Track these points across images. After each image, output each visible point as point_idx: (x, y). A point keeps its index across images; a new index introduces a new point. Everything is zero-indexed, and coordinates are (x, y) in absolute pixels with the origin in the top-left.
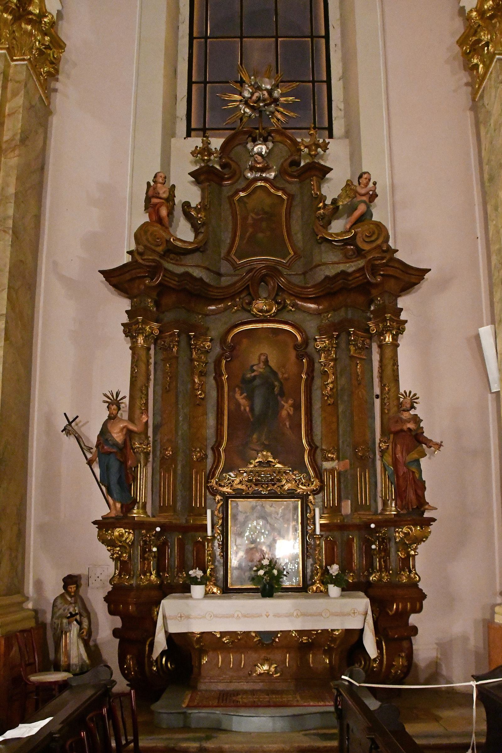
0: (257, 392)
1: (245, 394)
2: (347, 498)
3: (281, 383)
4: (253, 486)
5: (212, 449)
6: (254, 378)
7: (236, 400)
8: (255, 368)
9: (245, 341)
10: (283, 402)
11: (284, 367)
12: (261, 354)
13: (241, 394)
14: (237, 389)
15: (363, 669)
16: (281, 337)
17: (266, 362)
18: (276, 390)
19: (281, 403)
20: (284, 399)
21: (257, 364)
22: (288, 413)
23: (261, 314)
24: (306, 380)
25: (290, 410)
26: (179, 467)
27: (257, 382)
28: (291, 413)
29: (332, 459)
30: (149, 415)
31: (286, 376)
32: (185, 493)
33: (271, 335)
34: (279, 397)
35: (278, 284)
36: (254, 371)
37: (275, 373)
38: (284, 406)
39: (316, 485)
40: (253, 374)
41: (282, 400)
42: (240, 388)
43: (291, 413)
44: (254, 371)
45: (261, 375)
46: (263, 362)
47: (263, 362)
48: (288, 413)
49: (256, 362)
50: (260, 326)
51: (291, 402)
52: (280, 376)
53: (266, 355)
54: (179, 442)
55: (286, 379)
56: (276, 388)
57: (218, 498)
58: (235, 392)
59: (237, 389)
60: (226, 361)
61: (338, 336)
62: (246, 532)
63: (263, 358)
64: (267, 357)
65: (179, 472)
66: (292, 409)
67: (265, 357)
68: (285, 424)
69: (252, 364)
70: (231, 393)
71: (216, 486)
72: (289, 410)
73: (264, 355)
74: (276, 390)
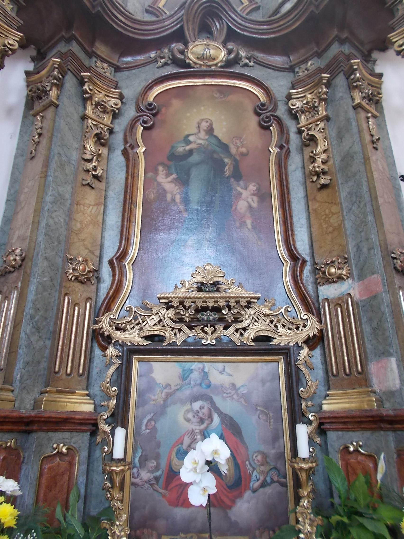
0: (194, 173)
1: (174, 176)
2: (386, 354)
3: (235, 160)
4: (185, 328)
5: (111, 263)
6: (191, 152)
7: (159, 184)
8: (191, 138)
9: (176, 103)
10: (239, 189)
11: (239, 138)
12: (202, 120)
13: (168, 175)
14: (160, 168)
15: (209, 343)
16: (234, 97)
17: (210, 131)
18: (228, 171)
19: (236, 190)
20: (241, 183)
21: (195, 134)
22: (250, 206)
23: (202, 63)
24: (278, 155)
25: (253, 201)
26: (32, 288)
27: (195, 158)
28: (255, 205)
29: (340, 278)
30: (290, 469)
31: (244, 150)
32: (41, 343)
33: (217, 95)
34: (232, 180)
35: (228, 25)
36: (190, 142)
37: (225, 147)
38: (241, 194)
39: (312, 328)
40: (188, 148)
41: (239, 185)
42: (168, 168)
43: (255, 205)
44: (190, 142)
45: (200, 149)
46: (205, 130)
47: (205, 130)
48: (250, 206)
49: (194, 130)
50: (199, 82)
51: (252, 187)
52: (233, 150)
53: (209, 121)
54: (40, 239)
55: (243, 155)
56: (227, 168)
57: (111, 351)
58: (156, 171)
59: (160, 168)
60: (145, 129)
61: (329, 80)
62: (368, 465)
63: (204, 125)
64: (211, 125)
65: (31, 296)
66: (255, 198)
67: (208, 124)
68: (245, 222)
69: (187, 133)
70: (150, 175)
71: (110, 329)
72: (250, 200)
73: (207, 122)
74: (228, 171)
